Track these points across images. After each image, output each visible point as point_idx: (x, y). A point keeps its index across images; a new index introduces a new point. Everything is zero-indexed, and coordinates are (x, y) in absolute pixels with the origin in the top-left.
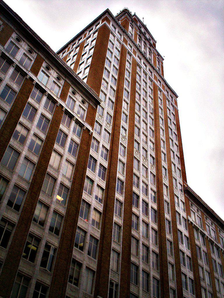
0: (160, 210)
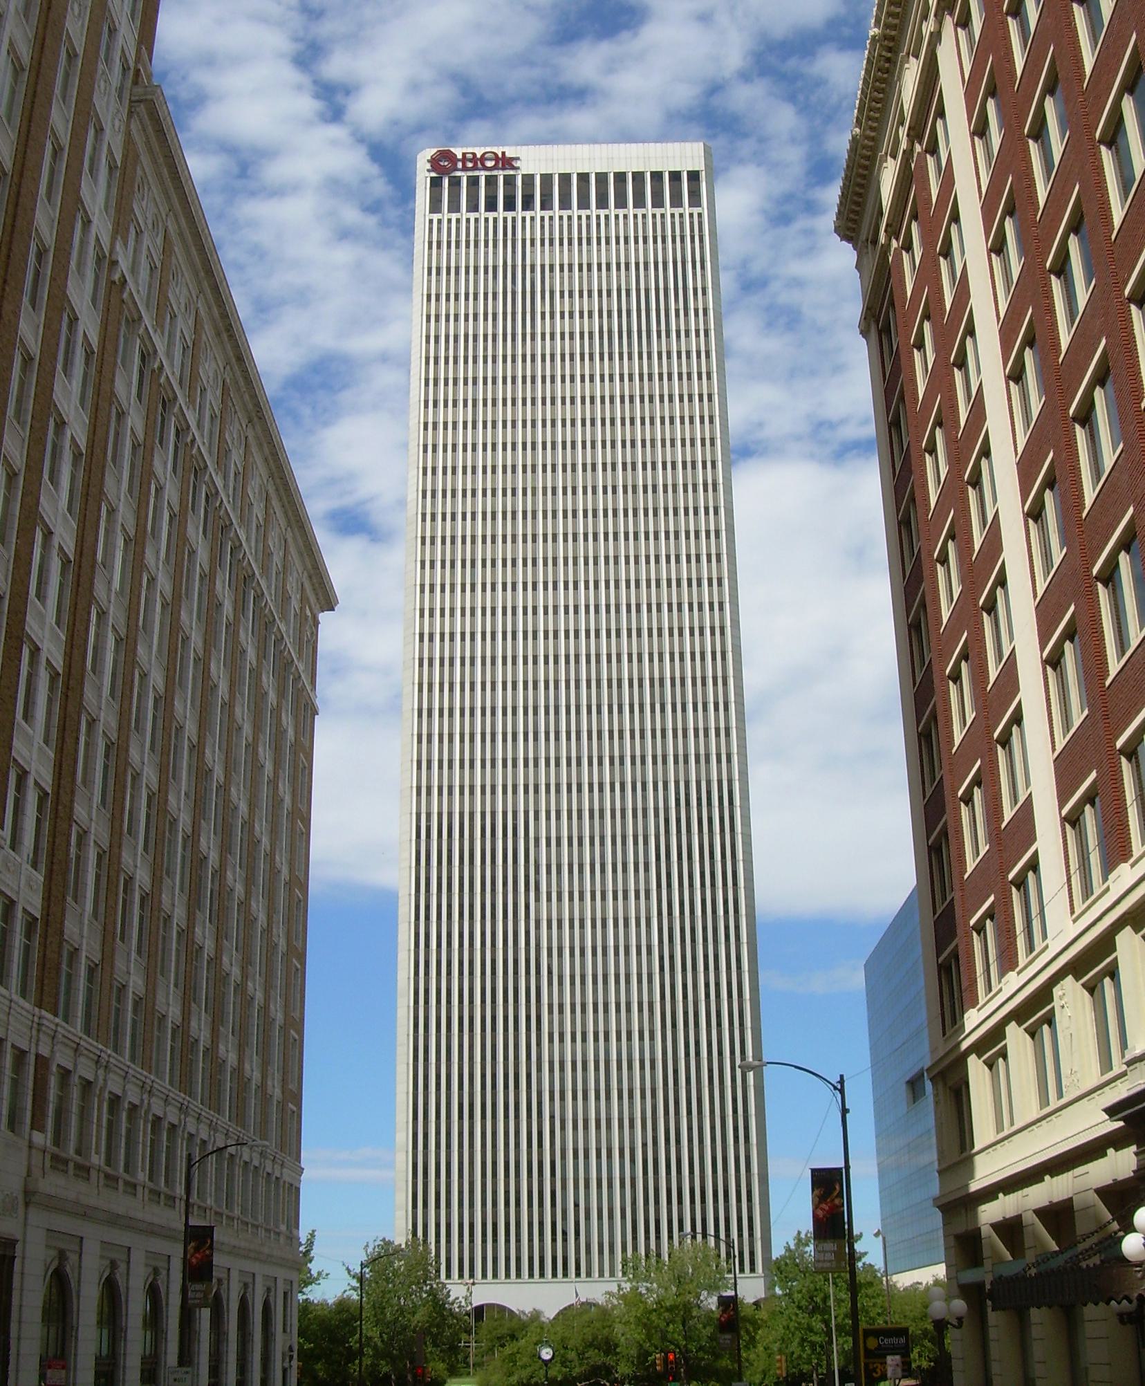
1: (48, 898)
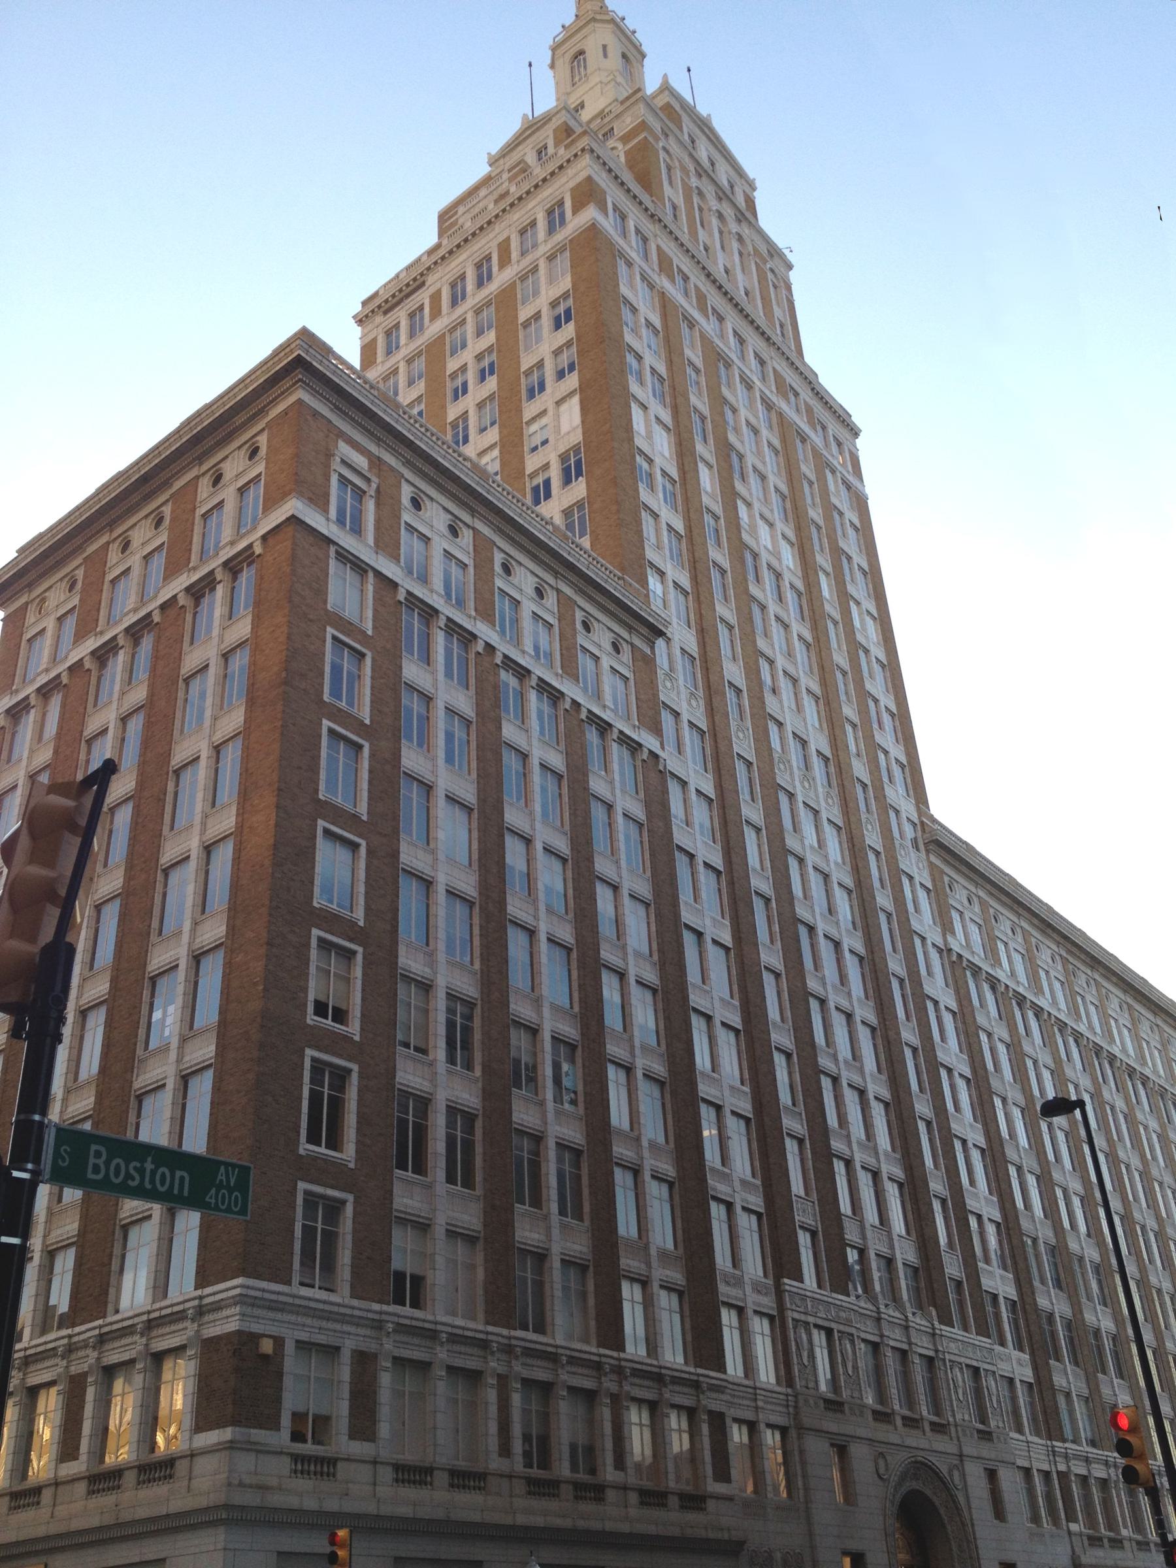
0: (872, 953)
1: (1035, 1368)
